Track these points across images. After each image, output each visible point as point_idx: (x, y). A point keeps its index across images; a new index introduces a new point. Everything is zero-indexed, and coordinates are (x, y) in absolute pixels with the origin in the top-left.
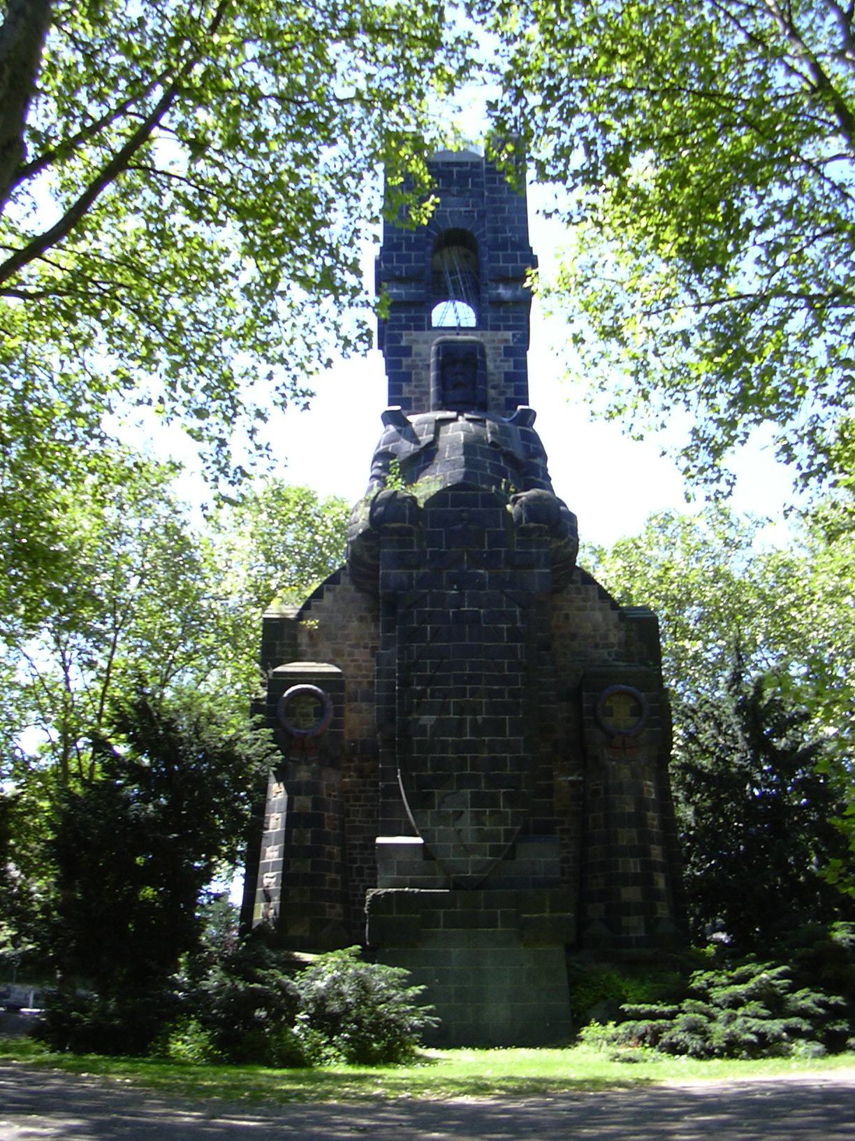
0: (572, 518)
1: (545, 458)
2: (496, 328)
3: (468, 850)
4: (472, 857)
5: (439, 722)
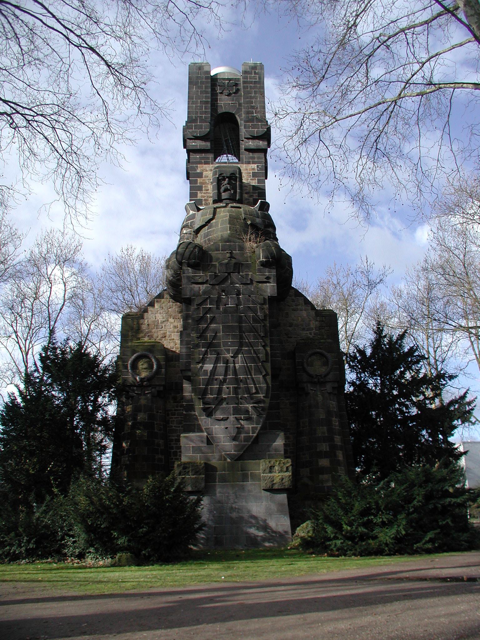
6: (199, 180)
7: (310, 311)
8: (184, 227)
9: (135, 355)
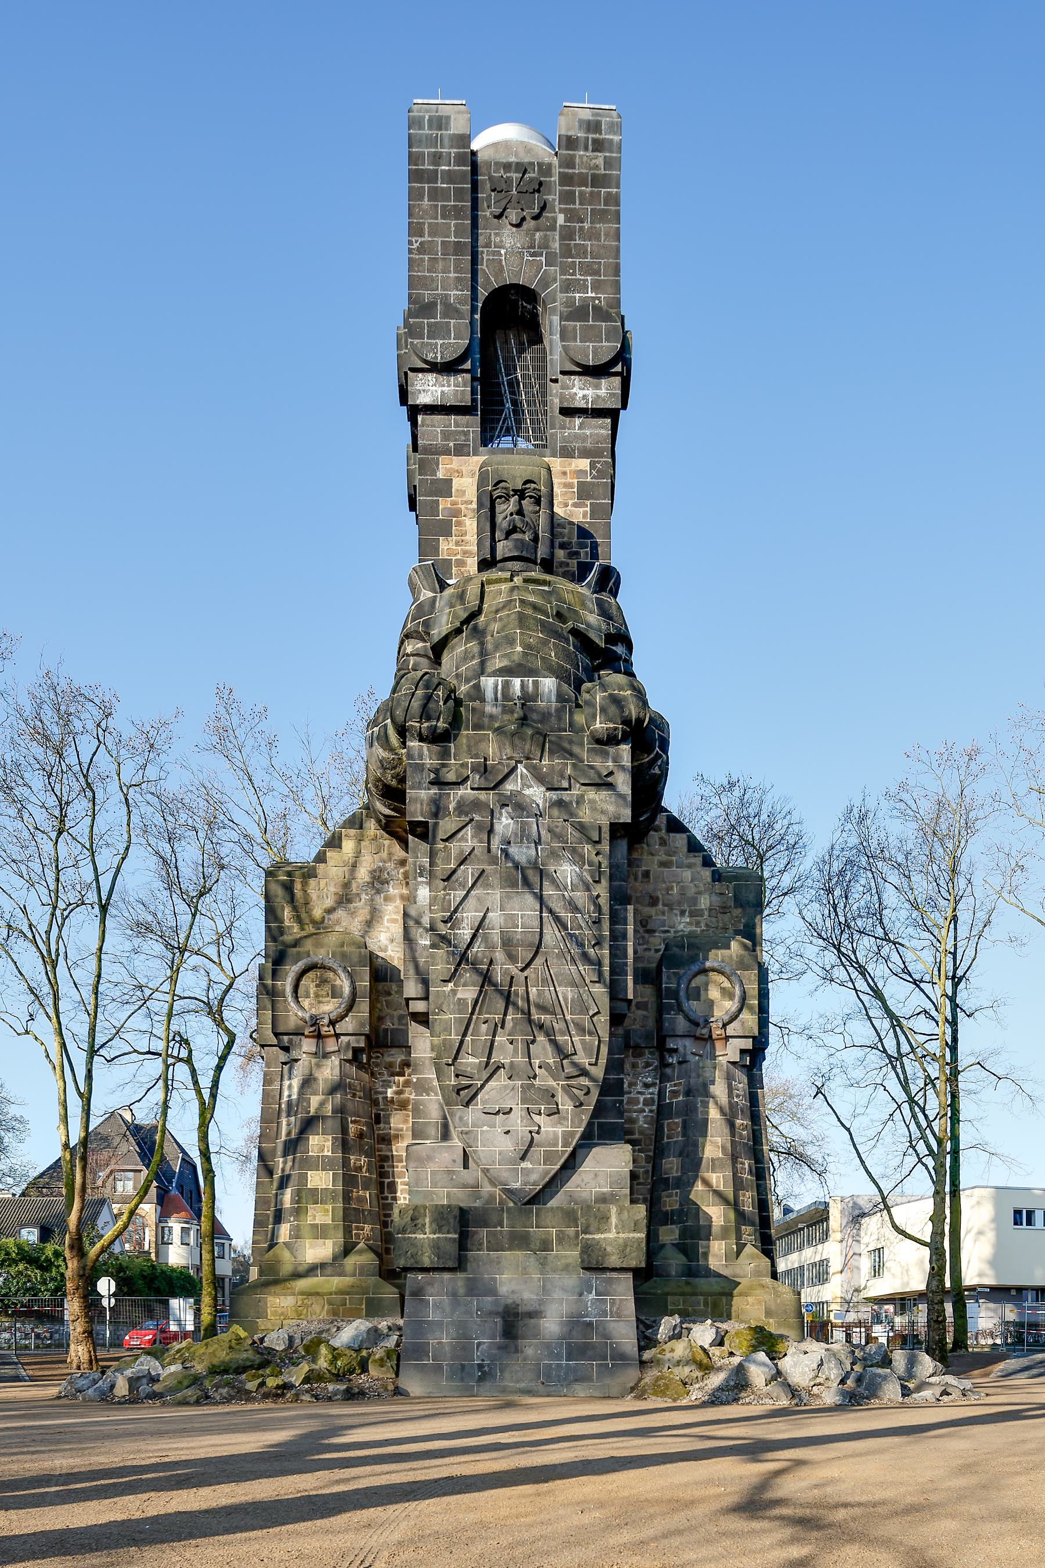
6: (444, 503)
7: (699, 868)
8: (407, 636)
9: (300, 964)
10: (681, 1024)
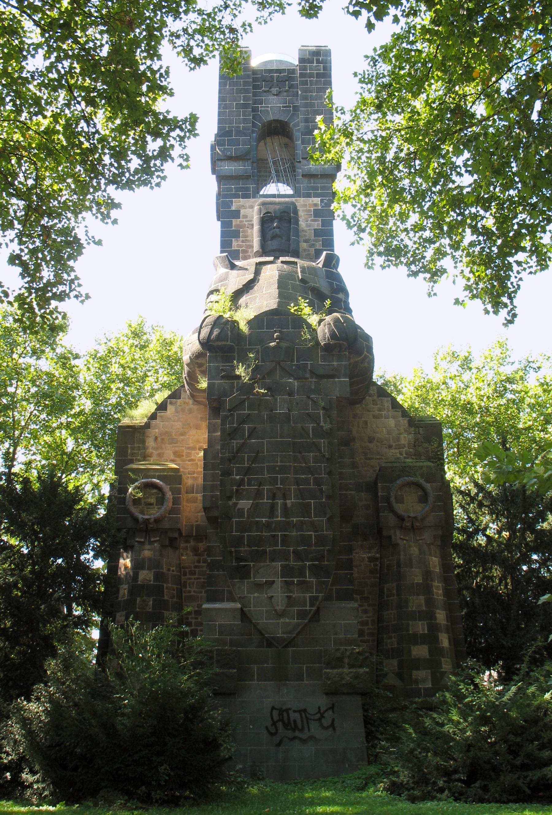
0: (368, 339)
1: (347, 294)
2: (308, 196)
3: (281, 615)
4: (282, 620)
5: (255, 506)
10: (392, 520)
